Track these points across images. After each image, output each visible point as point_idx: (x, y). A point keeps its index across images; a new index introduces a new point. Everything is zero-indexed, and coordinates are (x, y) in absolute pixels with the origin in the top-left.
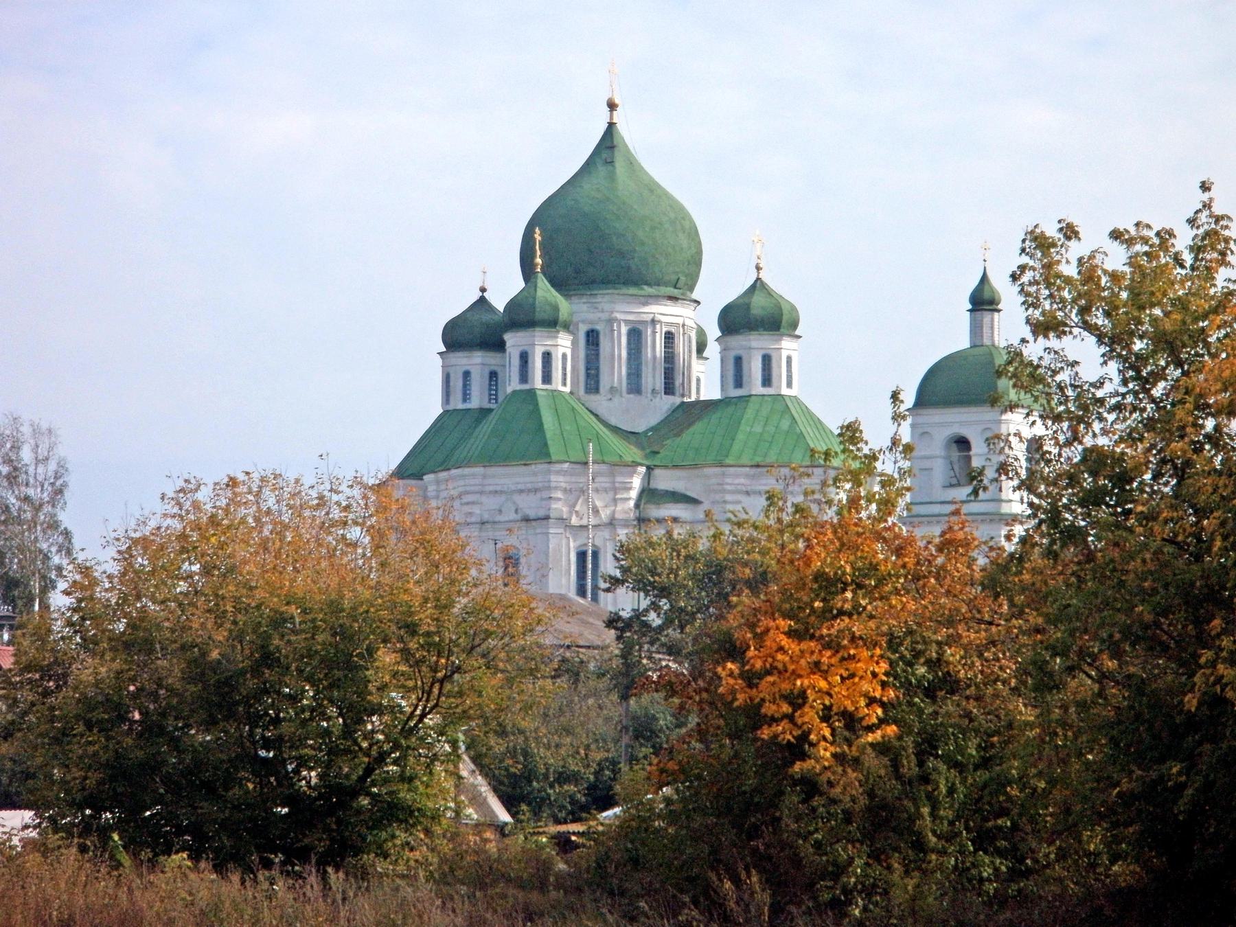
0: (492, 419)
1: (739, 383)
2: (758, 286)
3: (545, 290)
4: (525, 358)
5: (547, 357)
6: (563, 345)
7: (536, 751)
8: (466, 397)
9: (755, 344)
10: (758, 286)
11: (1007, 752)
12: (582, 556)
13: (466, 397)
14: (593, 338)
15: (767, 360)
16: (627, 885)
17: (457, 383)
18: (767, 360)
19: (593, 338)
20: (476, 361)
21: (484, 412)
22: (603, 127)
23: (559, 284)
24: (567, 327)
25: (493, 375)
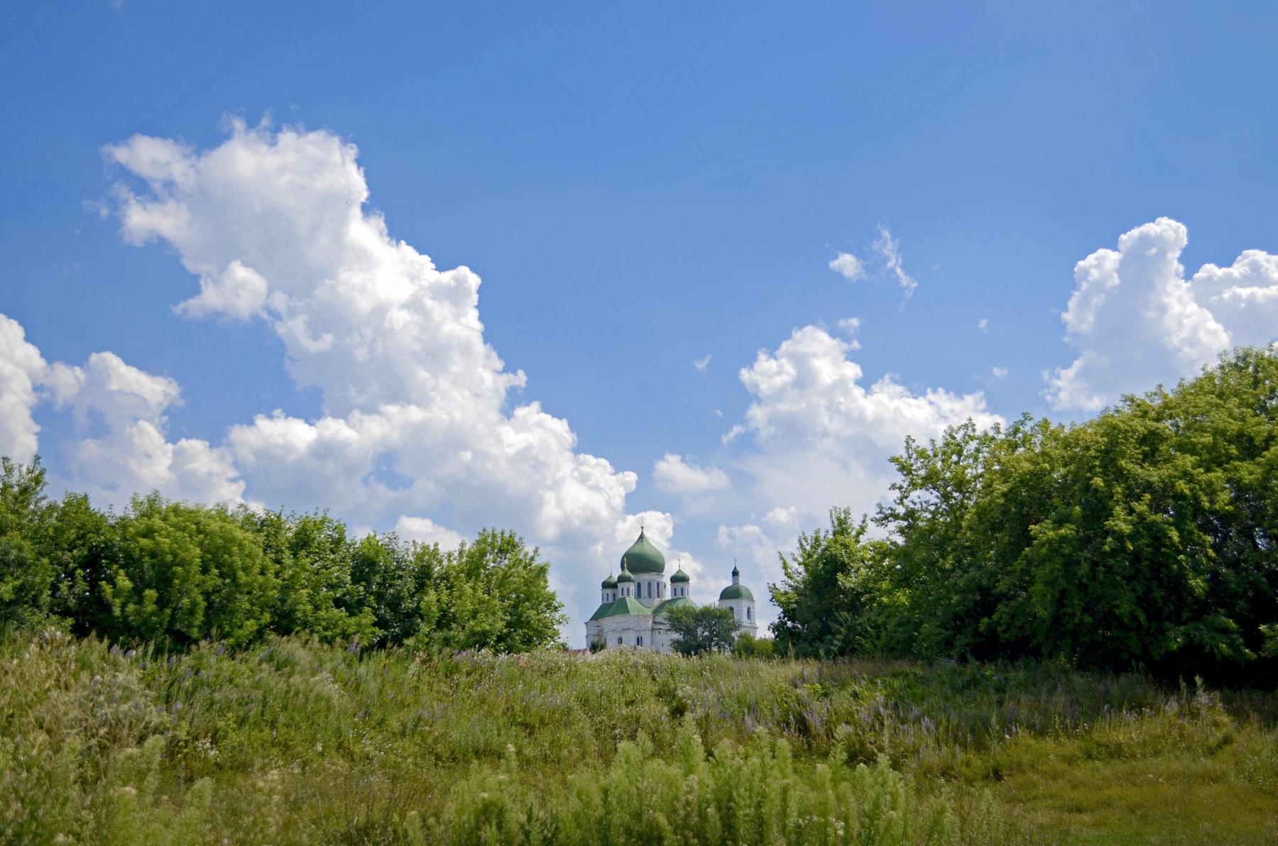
0: (615, 606)
1: (675, 595)
2: (679, 571)
3: (627, 573)
4: (622, 589)
5: (628, 589)
6: (632, 587)
7: (668, 736)
8: (608, 600)
9: (679, 585)
10: (679, 571)
11: (1271, 476)
12: (638, 638)
13: (608, 600)
14: (639, 585)
15: (682, 589)
16: (742, 762)
17: (605, 596)
18: (682, 589)
19: (639, 585)
20: (610, 591)
21: (612, 604)
22: (640, 533)
23: (631, 571)
24: (633, 581)
25: (614, 595)
